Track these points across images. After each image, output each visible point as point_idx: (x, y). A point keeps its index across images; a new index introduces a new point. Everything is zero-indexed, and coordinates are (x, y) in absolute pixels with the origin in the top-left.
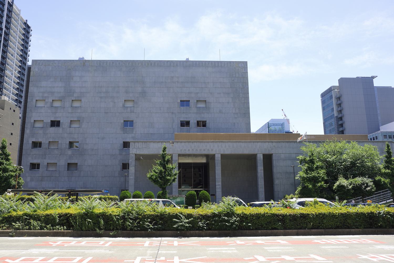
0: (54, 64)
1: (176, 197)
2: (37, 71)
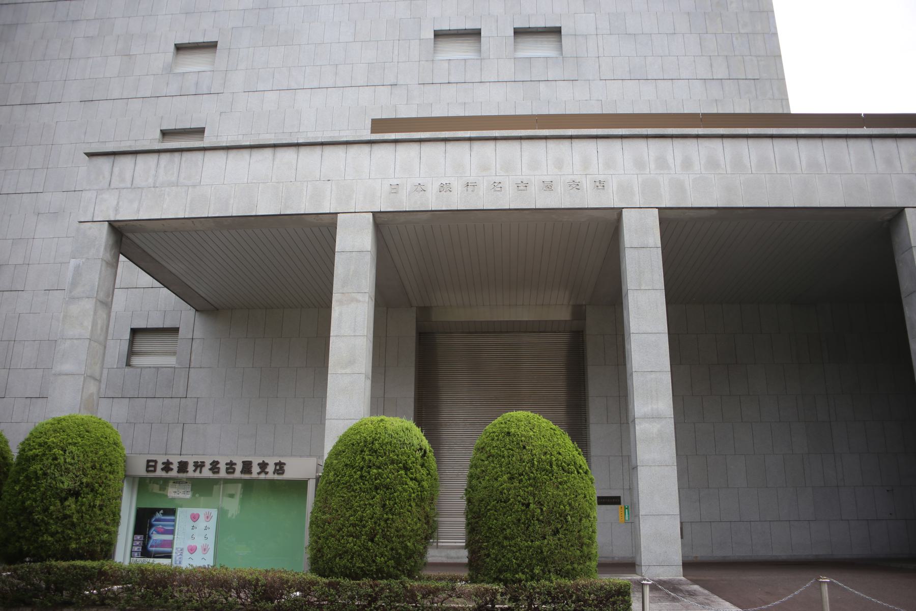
1: (223, 474)
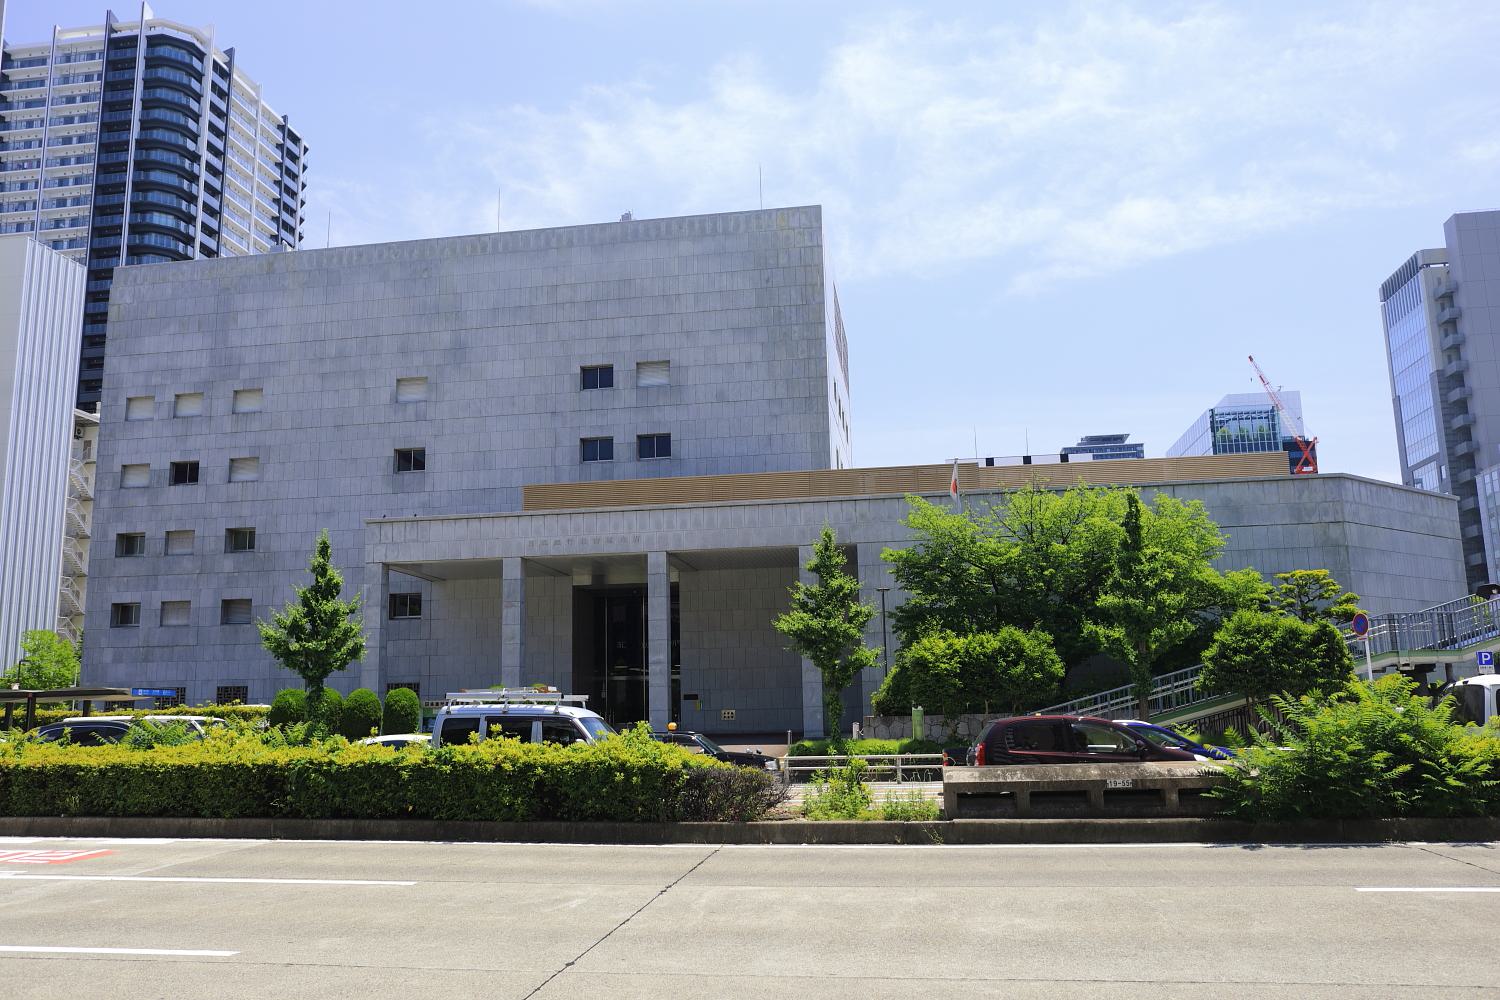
0: (181, 277)
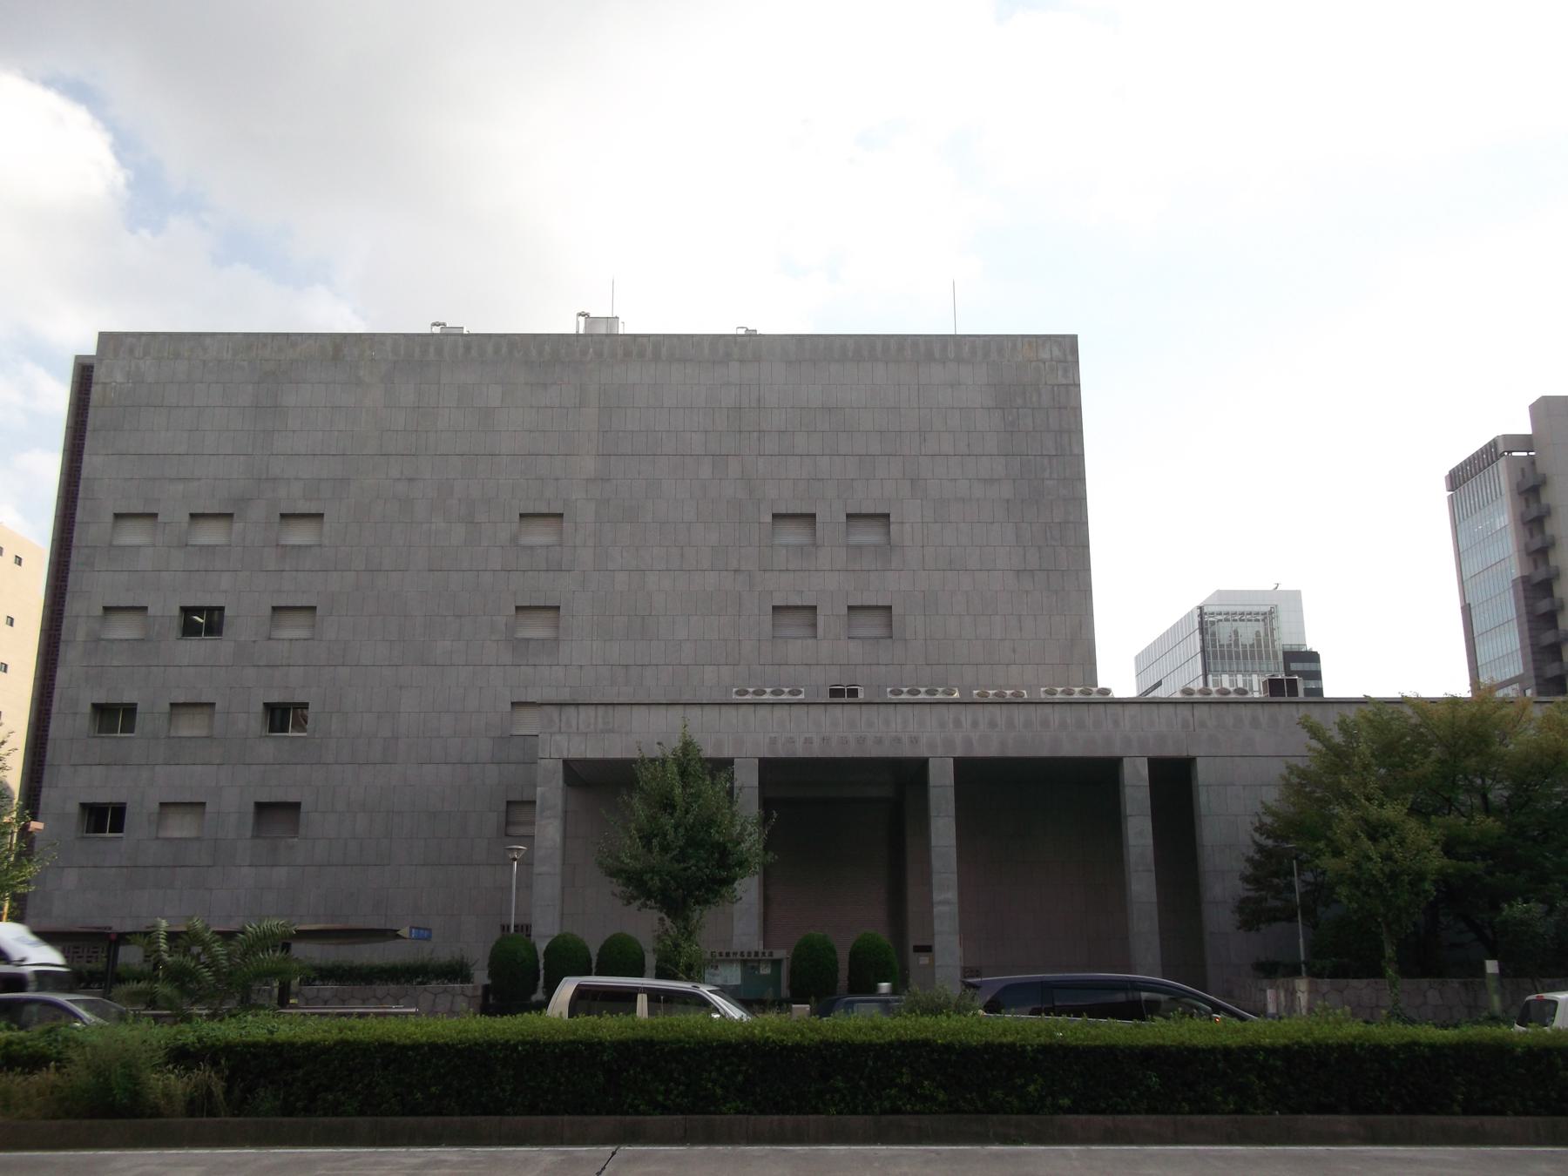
2: (121, 384)
